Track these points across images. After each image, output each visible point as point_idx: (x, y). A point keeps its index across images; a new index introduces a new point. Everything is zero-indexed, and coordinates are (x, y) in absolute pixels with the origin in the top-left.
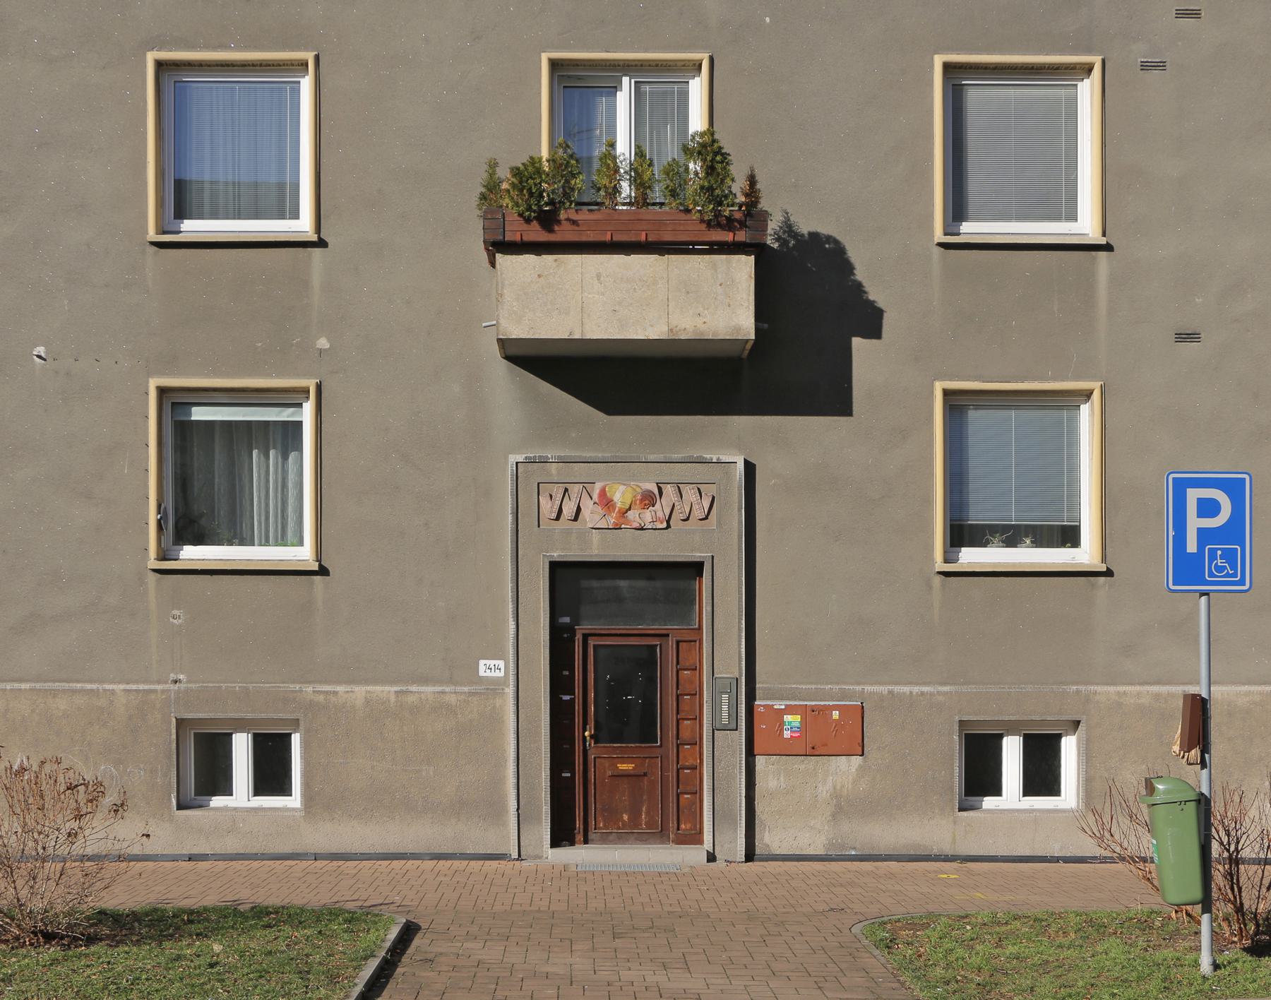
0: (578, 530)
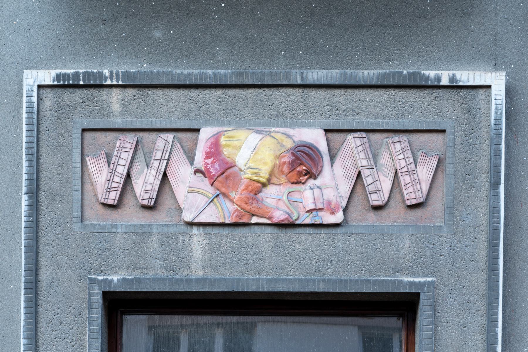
0: (164, 229)
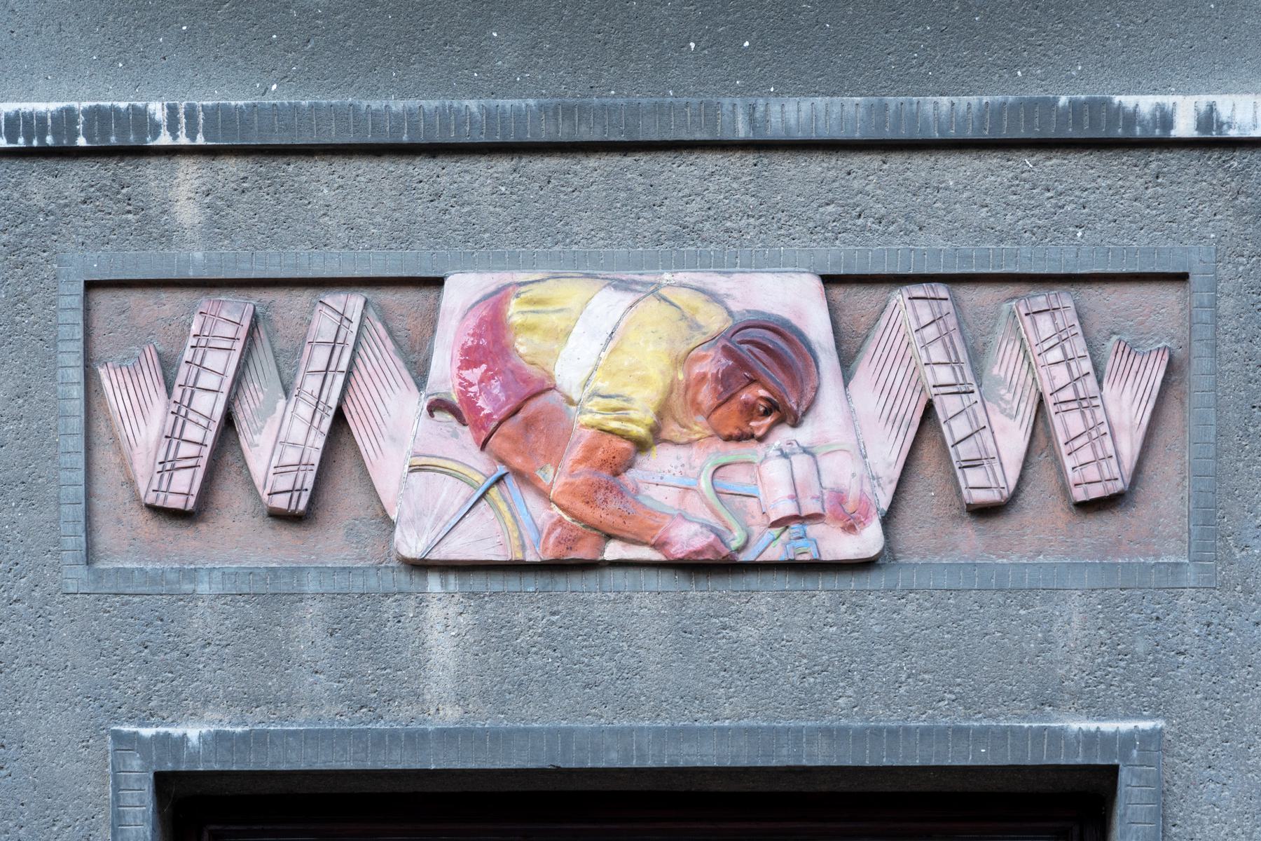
0: (341, 583)
